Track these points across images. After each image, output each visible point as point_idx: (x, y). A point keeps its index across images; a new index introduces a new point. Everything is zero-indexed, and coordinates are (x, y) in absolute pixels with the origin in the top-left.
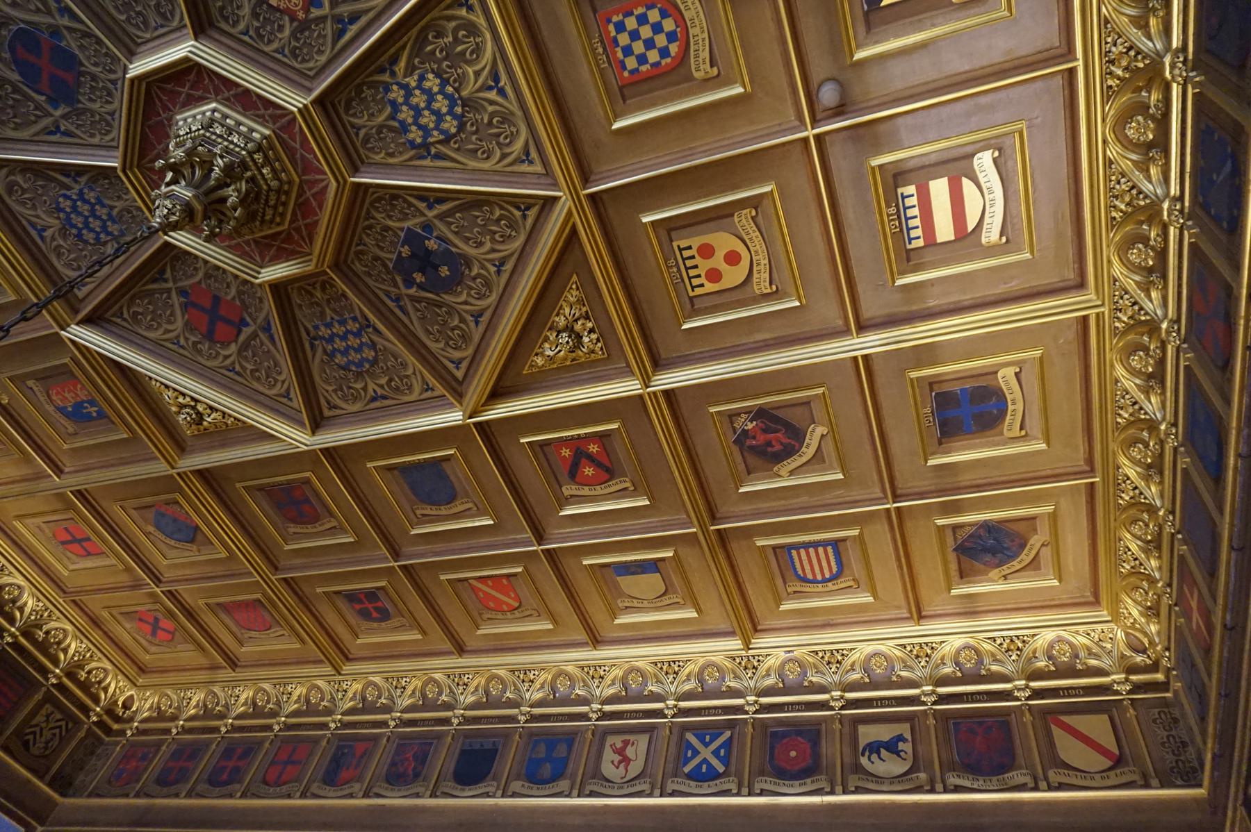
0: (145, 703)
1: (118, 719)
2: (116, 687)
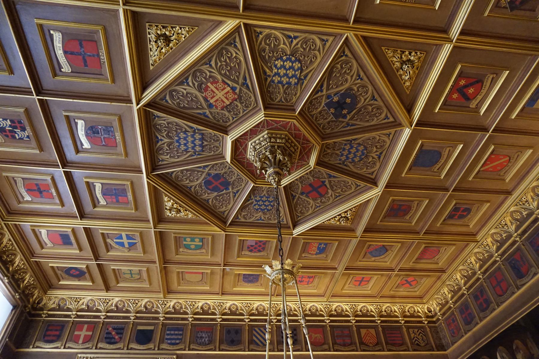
0: (434, 306)
1: (432, 317)
2: (421, 309)
